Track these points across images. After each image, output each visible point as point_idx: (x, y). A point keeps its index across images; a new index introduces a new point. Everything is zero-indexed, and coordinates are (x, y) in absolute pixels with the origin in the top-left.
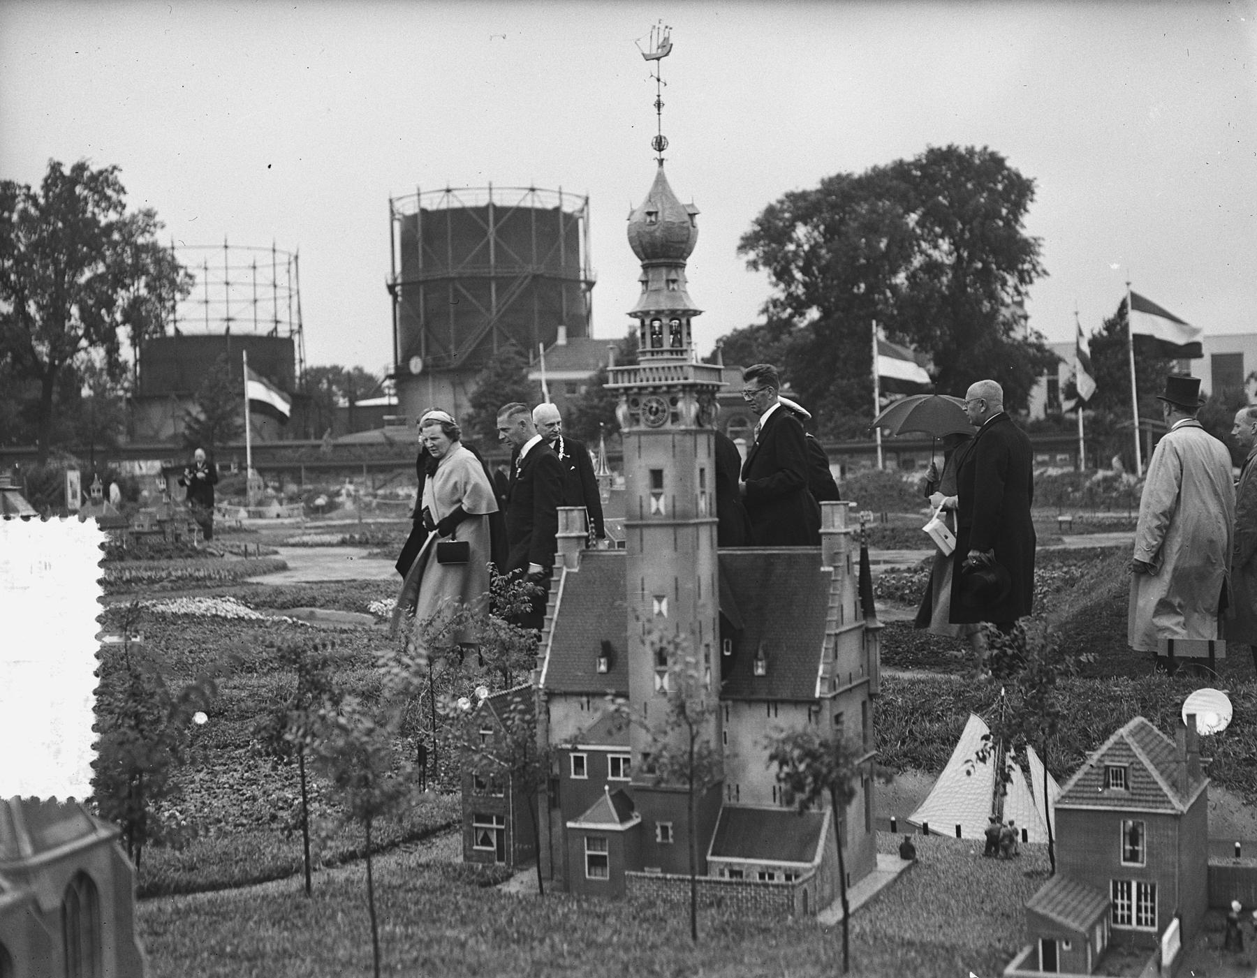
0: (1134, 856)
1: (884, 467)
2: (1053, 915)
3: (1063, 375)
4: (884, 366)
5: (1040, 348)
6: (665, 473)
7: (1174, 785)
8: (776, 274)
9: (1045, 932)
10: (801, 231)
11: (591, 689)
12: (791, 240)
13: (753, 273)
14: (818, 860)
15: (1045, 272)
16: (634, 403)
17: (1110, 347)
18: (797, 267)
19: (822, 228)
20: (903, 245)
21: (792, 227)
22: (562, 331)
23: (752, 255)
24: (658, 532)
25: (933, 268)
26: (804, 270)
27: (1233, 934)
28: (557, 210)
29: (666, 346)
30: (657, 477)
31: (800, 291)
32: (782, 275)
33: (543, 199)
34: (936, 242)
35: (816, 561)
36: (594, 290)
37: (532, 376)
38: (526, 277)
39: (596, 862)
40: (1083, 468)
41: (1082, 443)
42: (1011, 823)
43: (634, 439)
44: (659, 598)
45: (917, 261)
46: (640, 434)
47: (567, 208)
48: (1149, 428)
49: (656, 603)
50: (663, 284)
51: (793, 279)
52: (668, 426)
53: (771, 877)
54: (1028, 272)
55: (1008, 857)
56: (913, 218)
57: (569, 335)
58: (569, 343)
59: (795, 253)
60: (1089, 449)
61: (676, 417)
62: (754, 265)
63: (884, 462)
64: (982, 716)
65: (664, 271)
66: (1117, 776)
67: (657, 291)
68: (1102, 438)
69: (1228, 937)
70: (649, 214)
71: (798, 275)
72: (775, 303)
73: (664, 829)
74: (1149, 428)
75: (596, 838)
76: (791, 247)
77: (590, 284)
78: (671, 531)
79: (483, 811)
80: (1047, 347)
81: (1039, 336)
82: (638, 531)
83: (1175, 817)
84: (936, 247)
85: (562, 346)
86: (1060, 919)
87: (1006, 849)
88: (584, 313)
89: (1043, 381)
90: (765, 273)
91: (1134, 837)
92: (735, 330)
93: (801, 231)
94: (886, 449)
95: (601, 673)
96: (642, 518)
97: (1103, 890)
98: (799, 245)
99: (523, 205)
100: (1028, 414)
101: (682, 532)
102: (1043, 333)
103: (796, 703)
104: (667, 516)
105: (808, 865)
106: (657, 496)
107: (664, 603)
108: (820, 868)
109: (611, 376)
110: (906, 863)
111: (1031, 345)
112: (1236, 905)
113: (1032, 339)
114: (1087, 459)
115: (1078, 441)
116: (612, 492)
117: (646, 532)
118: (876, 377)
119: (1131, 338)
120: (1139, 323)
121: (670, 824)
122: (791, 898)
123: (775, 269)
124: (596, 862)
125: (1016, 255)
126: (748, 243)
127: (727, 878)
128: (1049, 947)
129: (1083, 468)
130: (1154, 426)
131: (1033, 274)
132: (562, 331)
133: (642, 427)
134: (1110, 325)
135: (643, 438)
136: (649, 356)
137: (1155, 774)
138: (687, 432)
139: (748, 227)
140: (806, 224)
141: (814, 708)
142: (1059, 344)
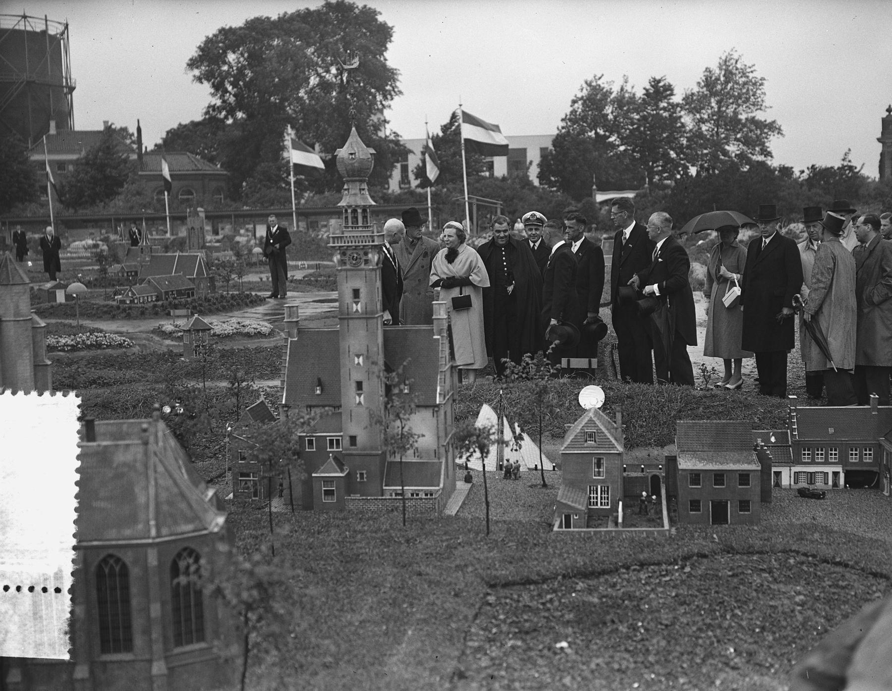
0: (599, 473)
1: (298, 226)
2: (570, 503)
3: (413, 161)
4: (296, 157)
5: (397, 143)
6: (361, 291)
7: (616, 439)
8: (214, 86)
9: (566, 511)
10: (231, 57)
11: (314, 403)
12: (225, 63)
13: (198, 84)
14: (441, 485)
15: (401, 92)
16: (343, 254)
17: (446, 142)
18: (230, 82)
19: (246, 55)
20: (303, 66)
21: (225, 53)
22: (53, 124)
23: (197, 72)
24: (357, 321)
25: (325, 85)
26: (234, 84)
27: (643, 506)
28: (44, 33)
29: (360, 224)
30: (356, 293)
31: (232, 99)
32: (219, 88)
33: (33, 25)
34: (328, 68)
35: (431, 332)
36: (74, 93)
37: (36, 157)
38: (22, 83)
39: (329, 493)
40: (430, 229)
41: (430, 210)
42: (508, 461)
43: (343, 273)
44: (358, 356)
45: (313, 81)
46: (346, 270)
47: (52, 31)
48: (474, 201)
49: (356, 359)
50: (358, 191)
51: (226, 91)
52: (363, 266)
53: (417, 495)
54: (390, 91)
55: (516, 479)
56: (311, 50)
57: (58, 127)
58: (58, 134)
59: (228, 72)
60: (434, 215)
61: (367, 262)
62: (199, 79)
63: (298, 221)
64: (490, 405)
65: (358, 184)
66: (591, 436)
67: (355, 194)
68: (441, 206)
69: (641, 508)
70: (352, 154)
71: (230, 88)
72: (213, 107)
73: (362, 474)
74: (474, 201)
75: (328, 481)
76: (225, 68)
77: (72, 89)
78: (364, 321)
79: (245, 471)
80: (402, 143)
81: (397, 135)
82: (346, 321)
83: (619, 454)
84: (328, 71)
85: (53, 135)
86: (573, 505)
87: (515, 475)
88: (67, 110)
89: (399, 165)
90: (206, 87)
91: (599, 465)
92: (180, 124)
93: (231, 57)
94: (299, 214)
95: (318, 395)
96: (348, 314)
97: (584, 490)
98: (231, 67)
99: (17, 27)
100: (388, 188)
101: (370, 321)
102: (399, 133)
103: (426, 407)
104: (362, 314)
105: (437, 488)
106: (357, 303)
107: (361, 358)
108: (443, 489)
109: (331, 240)
110: (470, 485)
111: (392, 141)
112: (644, 493)
113: (392, 137)
114: (433, 221)
115: (427, 209)
116: (152, 257)
117: (350, 321)
118: (291, 164)
119: (463, 142)
120: (468, 132)
121: (364, 472)
122: (434, 504)
123: (213, 84)
124: (329, 493)
125: (381, 80)
126: (193, 64)
127: (394, 497)
128: (568, 518)
129: (430, 229)
130: (478, 200)
131: (393, 93)
132: (53, 124)
133: (348, 267)
134: (445, 128)
135: (349, 273)
136: (350, 229)
137: (608, 435)
138: (373, 269)
139: (193, 52)
140: (234, 52)
141: (436, 409)
142: (410, 140)
